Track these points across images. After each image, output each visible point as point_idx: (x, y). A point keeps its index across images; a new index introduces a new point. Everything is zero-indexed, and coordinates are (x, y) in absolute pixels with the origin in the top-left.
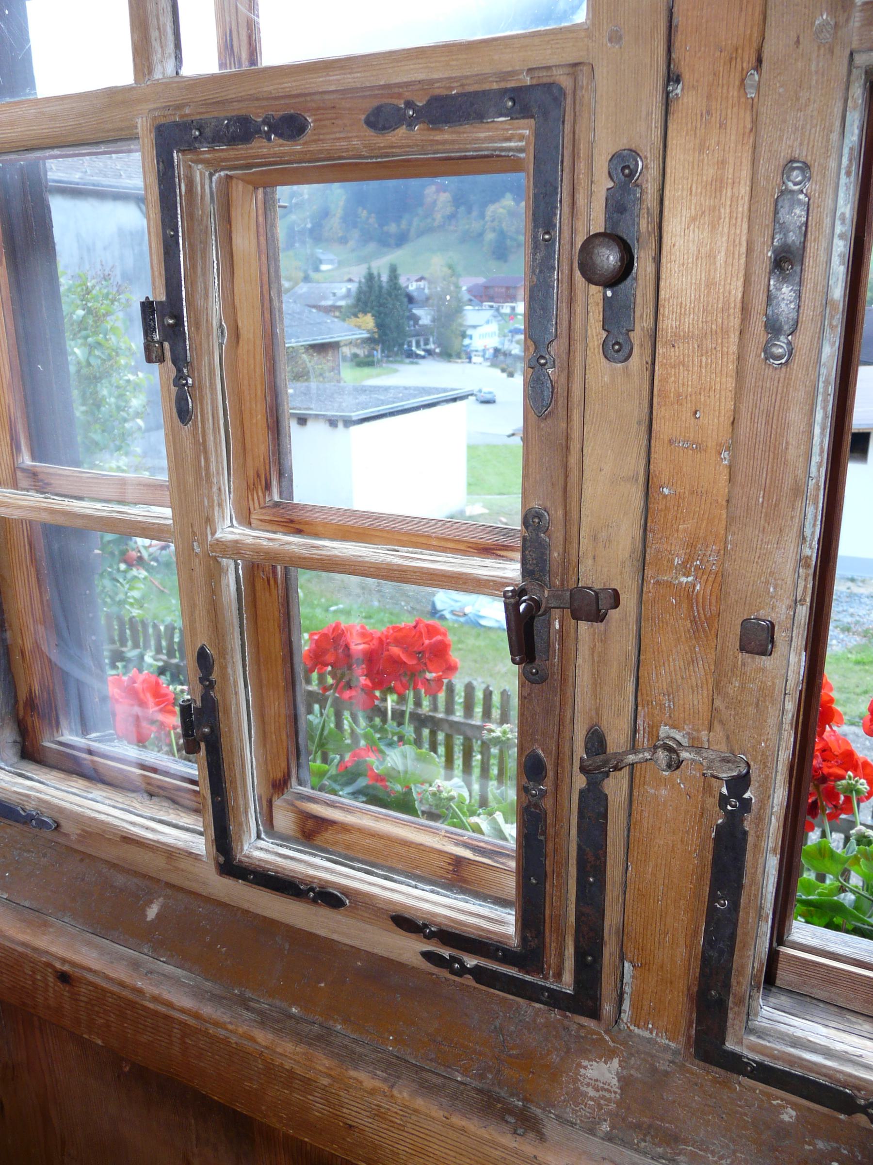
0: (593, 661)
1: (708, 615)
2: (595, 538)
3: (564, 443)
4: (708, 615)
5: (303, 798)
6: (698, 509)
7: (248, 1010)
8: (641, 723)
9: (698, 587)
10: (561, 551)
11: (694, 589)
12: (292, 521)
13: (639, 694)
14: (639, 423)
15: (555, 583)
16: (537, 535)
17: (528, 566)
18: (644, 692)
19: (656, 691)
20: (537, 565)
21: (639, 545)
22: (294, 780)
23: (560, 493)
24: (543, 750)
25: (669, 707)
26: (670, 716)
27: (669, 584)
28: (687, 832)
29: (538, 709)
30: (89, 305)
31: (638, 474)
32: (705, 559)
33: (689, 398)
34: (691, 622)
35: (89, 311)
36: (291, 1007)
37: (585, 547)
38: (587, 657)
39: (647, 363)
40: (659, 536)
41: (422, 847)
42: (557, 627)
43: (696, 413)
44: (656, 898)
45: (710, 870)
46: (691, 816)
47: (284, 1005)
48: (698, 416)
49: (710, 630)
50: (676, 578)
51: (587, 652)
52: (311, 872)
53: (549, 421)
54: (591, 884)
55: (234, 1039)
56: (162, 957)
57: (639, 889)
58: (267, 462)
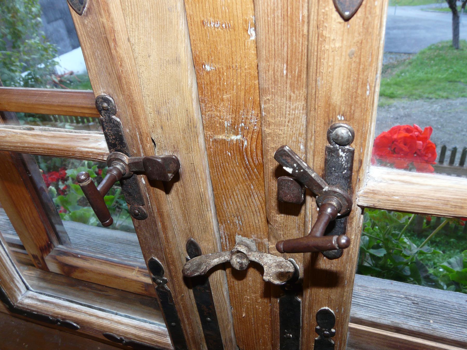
1: (257, 163)
2: (159, 113)
4: (257, 163)
5: (61, 253)
9: (246, 143)
11: (243, 145)
16: (109, 117)
19: (229, 214)
20: (116, 139)
22: (55, 243)
24: (158, 258)
26: (241, 230)
27: (223, 142)
29: (148, 235)
32: (248, 121)
34: (245, 168)
45: (279, 318)
49: (260, 174)
52: (57, 310)
54: (209, 322)
57: (240, 319)
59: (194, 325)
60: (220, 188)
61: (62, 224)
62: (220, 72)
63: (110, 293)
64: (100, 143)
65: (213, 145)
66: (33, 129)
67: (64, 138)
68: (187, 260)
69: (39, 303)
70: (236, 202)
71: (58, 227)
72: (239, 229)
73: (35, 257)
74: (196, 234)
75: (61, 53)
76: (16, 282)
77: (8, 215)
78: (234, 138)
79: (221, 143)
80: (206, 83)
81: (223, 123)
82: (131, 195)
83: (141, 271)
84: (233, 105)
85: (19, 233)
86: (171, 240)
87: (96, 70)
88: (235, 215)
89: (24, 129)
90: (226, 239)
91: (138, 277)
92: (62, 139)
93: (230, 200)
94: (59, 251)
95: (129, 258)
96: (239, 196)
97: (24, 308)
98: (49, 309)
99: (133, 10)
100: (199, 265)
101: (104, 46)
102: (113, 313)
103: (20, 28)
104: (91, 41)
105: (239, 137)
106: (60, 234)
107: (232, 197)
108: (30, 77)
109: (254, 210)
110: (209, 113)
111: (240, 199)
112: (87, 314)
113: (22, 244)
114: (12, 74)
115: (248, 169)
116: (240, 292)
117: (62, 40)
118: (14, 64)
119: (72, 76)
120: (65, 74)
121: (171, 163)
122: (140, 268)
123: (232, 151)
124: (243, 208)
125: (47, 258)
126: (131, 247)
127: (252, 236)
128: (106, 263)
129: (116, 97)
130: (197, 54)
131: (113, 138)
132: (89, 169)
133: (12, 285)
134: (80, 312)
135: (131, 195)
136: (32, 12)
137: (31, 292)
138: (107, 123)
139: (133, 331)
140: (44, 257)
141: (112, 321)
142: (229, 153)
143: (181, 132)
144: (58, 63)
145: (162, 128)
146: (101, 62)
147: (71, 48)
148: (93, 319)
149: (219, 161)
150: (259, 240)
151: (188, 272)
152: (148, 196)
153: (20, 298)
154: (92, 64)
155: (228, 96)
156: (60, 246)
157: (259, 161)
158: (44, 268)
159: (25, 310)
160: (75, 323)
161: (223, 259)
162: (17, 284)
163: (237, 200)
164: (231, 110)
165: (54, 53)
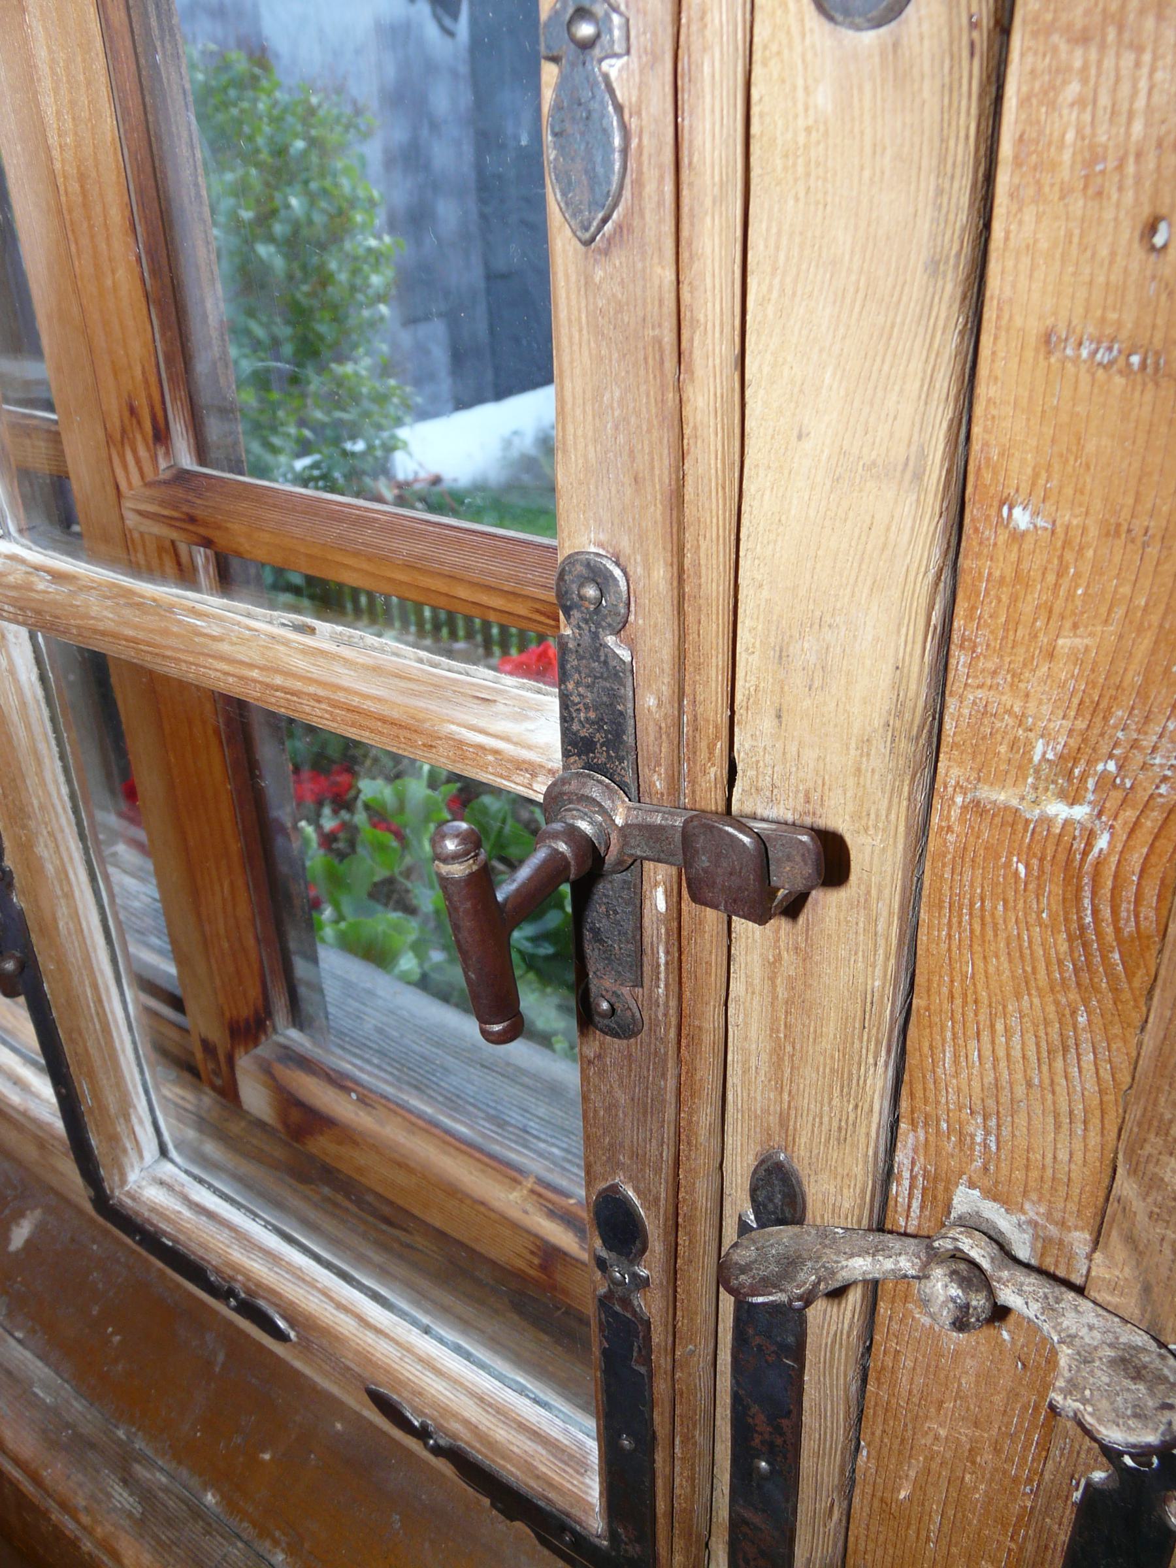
0: (775, 997)
1: (1130, 928)
2: (782, 656)
3: (669, 338)
4: (1130, 928)
5: (290, 1058)
6: (1126, 590)
7: (125, 1482)
8: (907, 1162)
9: (1102, 842)
10: (666, 690)
11: (1089, 845)
12: (192, 519)
13: (904, 1092)
14: (934, 267)
15: (651, 784)
16: (595, 636)
17: (575, 727)
18: (918, 1088)
19: (952, 1097)
20: (598, 723)
21: (918, 689)
22: (281, 1017)
23: (656, 513)
24: (637, 1190)
25: (986, 1146)
26: (986, 1169)
27: (1011, 819)
28: (1013, 1437)
29: (622, 1098)
30: (313, 132)
31: (922, 455)
32: (1138, 758)
33: (1131, 169)
34: (1070, 939)
35: (313, 142)
36: (205, 1490)
37: (753, 680)
38: (757, 981)
39: (973, 26)
40: (990, 665)
41: (482, 1209)
42: (662, 906)
43: (1152, 229)
44: (924, 1533)
46: (1025, 1408)
47: (195, 1482)
48: (1159, 240)
49: (1130, 975)
50: (1035, 802)
51: (758, 972)
52: (238, 1255)
53: (618, 258)
54: (764, 1478)
55: (87, 1546)
56: (19, 1328)
57: (882, 1500)
58: (153, 379)
59: (702, 1473)
60: (945, 990)
61: (314, 959)
62: (1066, 543)
63: (419, 1241)
64: (529, 725)
65: (962, 819)
66: (312, 631)
67: (410, 679)
68: (744, 1228)
69: (187, 1213)
70: (996, 1060)
71: (301, 968)
72: (979, 1163)
73: (208, 1048)
74: (803, 1140)
75: (423, 415)
76: (134, 1120)
77: (161, 886)
78: (1058, 810)
79: (998, 820)
80: (997, 574)
81: (1029, 746)
82: (601, 941)
83: (540, 1195)
84: (1091, 684)
85: (180, 958)
86: (702, 1139)
87: (591, 455)
88: (978, 1107)
89: (284, 625)
90: (912, 1187)
91: (526, 1212)
92: (403, 684)
93: (973, 1044)
94: (286, 1047)
95: (499, 1126)
96: (1017, 1038)
97: (137, 1213)
98: (212, 1244)
99: (782, 256)
100: (791, 1264)
101: (642, 372)
102: (415, 1322)
103: (322, 328)
104: (599, 346)
105: (1080, 812)
106: (302, 991)
107: (986, 1036)
108: (316, 473)
109: (1064, 1108)
110: (980, 693)
111: (1017, 1053)
112: (331, 1299)
113: (178, 992)
114: (268, 458)
115: (1085, 945)
116: (915, 1400)
117: (431, 377)
118: (281, 429)
119: (437, 489)
120: (416, 480)
121: (789, 858)
122: (540, 1181)
123: (1035, 862)
124: (1020, 1091)
125: (244, 1062)
126: (515, 1090)
127: (1027, 1206)
128: (427, 1131)
129: (637, 570)
130: (988, 459)
131: (587, 719)
132: (429, 792)
133: (121, 1128)
134: (311, 1284)
135: (601, 941)
136: (369, 286)
137: (169, 1166)
138: (580, 658)
139: (472, 1411)
140: (237, 1056)
141: (408, 1350)
142: (1022, 869)
143: (853, 745)
144: (405, 445)
145: (779, 717)
146: (616, 428)
147: (450, 405)
148: (345, 1325)
149: (972, 886)
150: (1053, 1230)
151: (742, 1277)
152: (662, 960)
153: (133, 1177)
154: (580, 432)
155: (1078, 641)
156: (294, 1034)
157: (1143, 924)
158: (229, 1093)
159: (139, 1221)
160: (284, 1318)
161: (889, 1264)
162: (137, 1128)
163: (1001, 1053)
164: (1076, 701)
165: (400, 413)
